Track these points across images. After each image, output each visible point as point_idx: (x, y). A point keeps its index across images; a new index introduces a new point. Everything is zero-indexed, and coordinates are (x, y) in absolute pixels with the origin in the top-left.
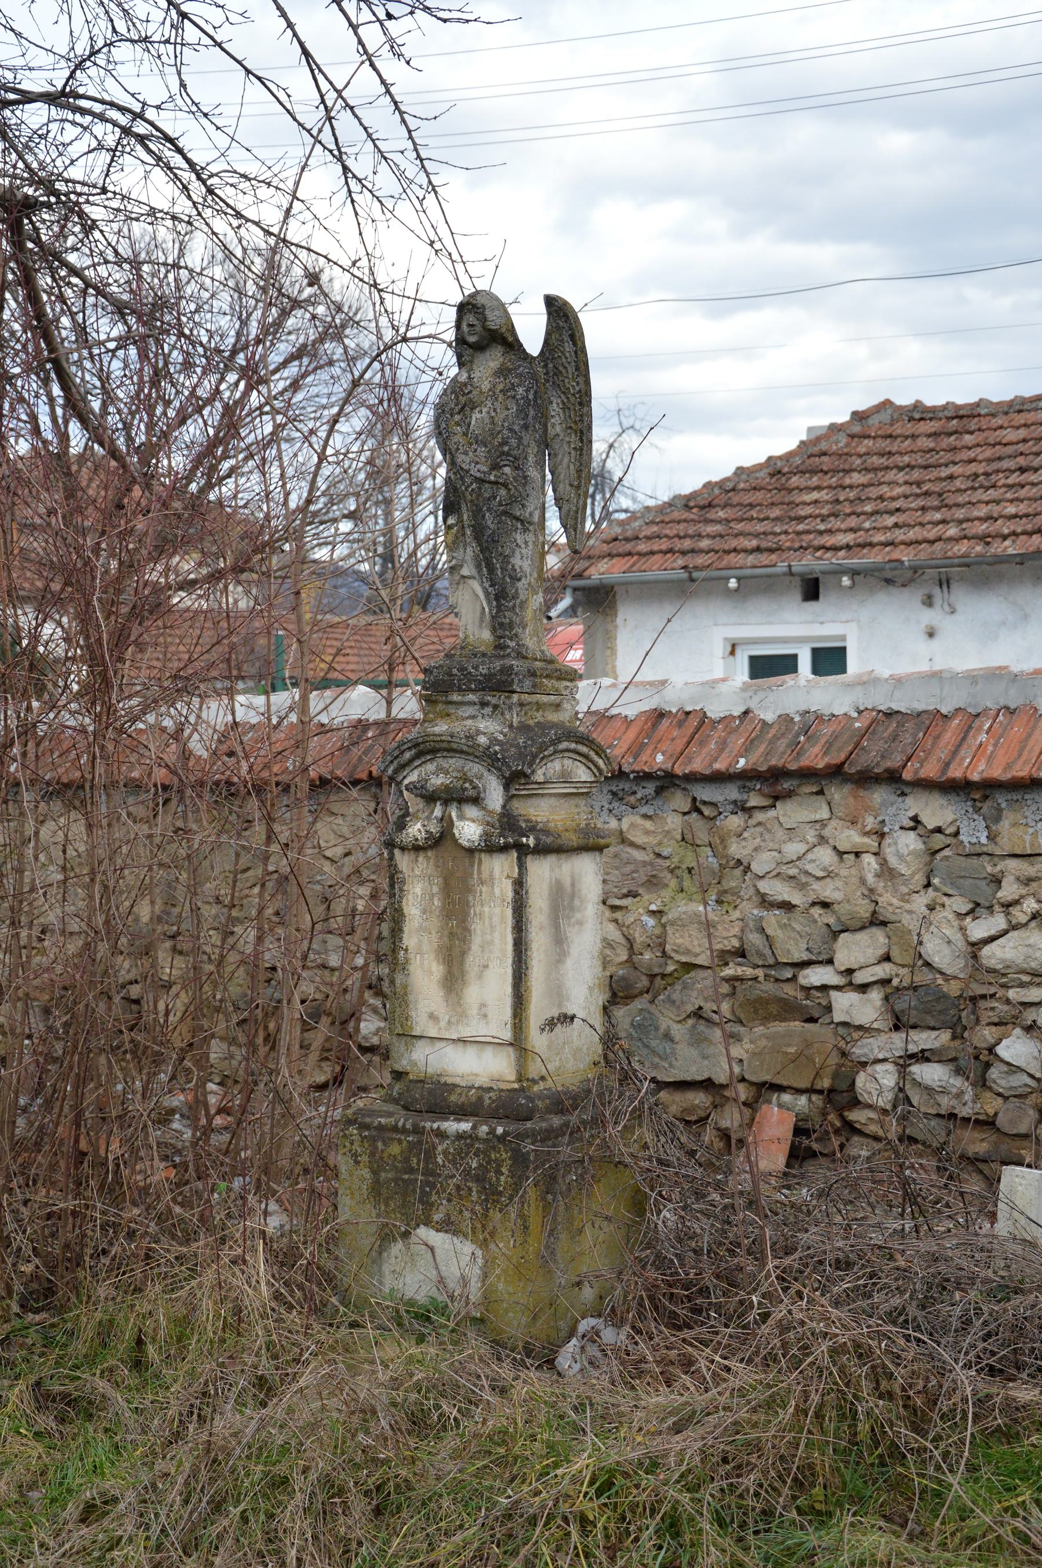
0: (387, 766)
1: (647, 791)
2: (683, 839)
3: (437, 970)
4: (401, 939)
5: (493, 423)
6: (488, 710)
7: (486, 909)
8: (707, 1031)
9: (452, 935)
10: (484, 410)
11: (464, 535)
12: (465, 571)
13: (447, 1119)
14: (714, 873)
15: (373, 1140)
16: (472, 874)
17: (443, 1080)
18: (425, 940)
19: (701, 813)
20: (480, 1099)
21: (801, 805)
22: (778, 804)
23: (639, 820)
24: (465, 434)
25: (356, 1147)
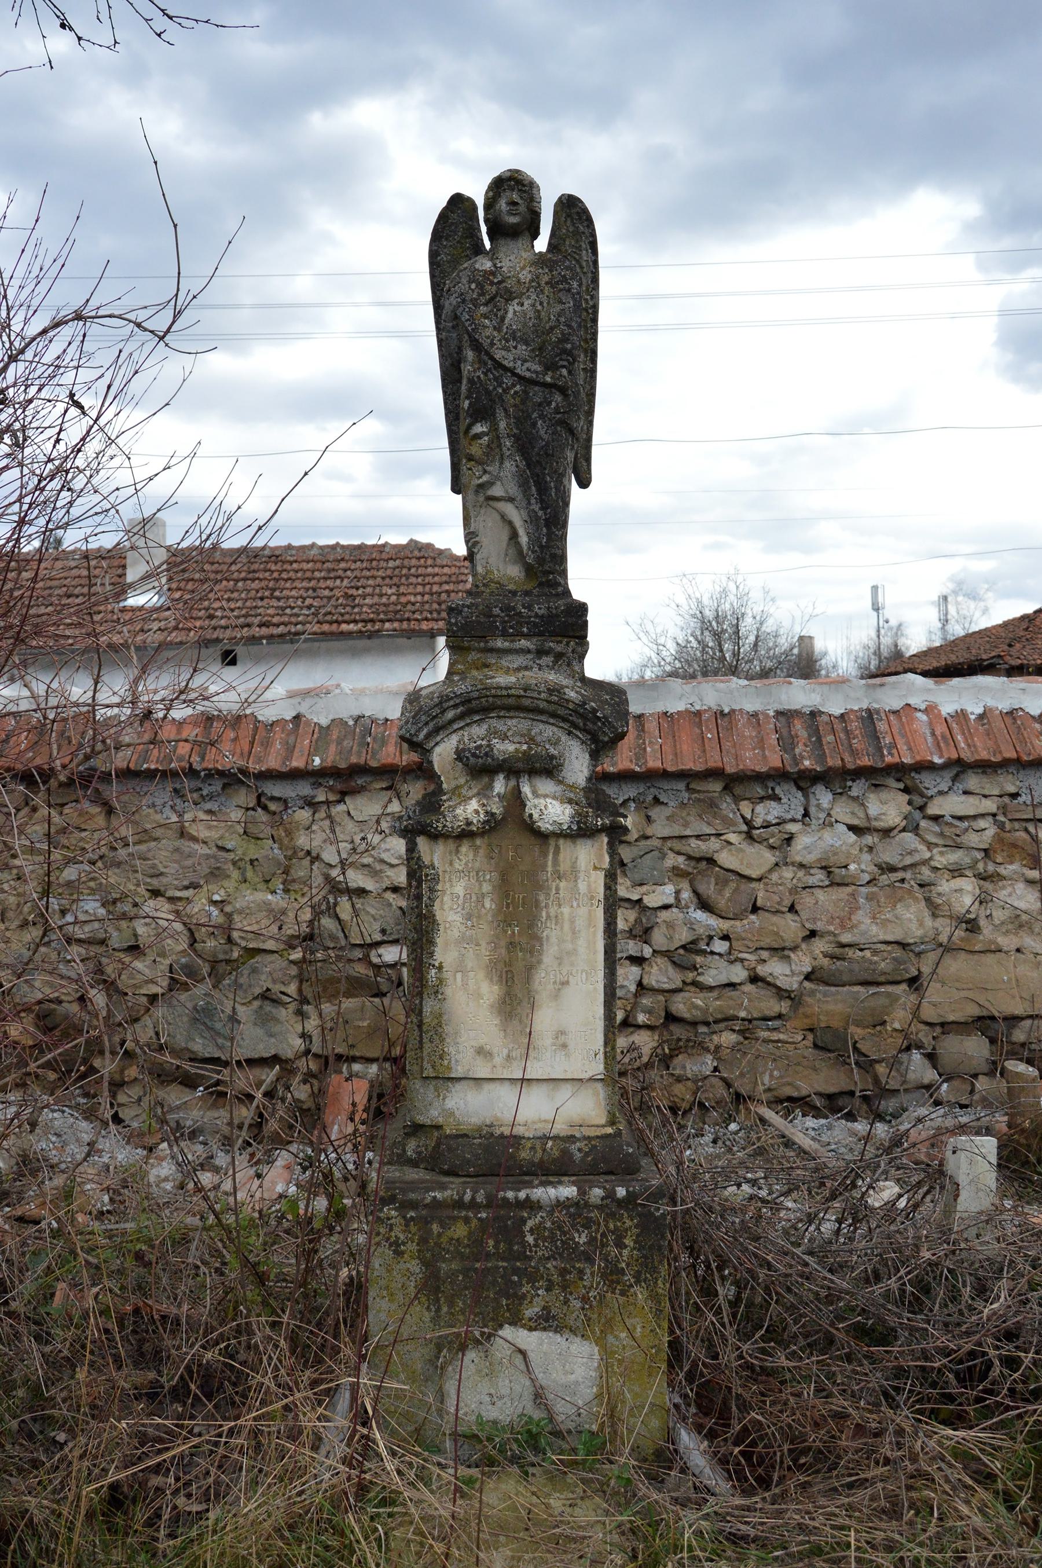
0: (420, 730)
1: (213, 788)
2: (245, 832)
3: (490, 991)
5: (538, 318)
6: (547, 660)
7: (566, 910)
8: (274, 1011)
9: (512, 945)
10: (527, 303)
11: (500, 446)
12: (497, 491)
13: (530, 1185)
14: (279, 864)
15: (426, 1222)
16: (545, 865)
17: (497, 1132)
18: (470, 954)
19: (265, 808)
21: (370, 799)
22: (347, 799)
23: (202, 816)
24: (498, 329)
25: (397, 1232)
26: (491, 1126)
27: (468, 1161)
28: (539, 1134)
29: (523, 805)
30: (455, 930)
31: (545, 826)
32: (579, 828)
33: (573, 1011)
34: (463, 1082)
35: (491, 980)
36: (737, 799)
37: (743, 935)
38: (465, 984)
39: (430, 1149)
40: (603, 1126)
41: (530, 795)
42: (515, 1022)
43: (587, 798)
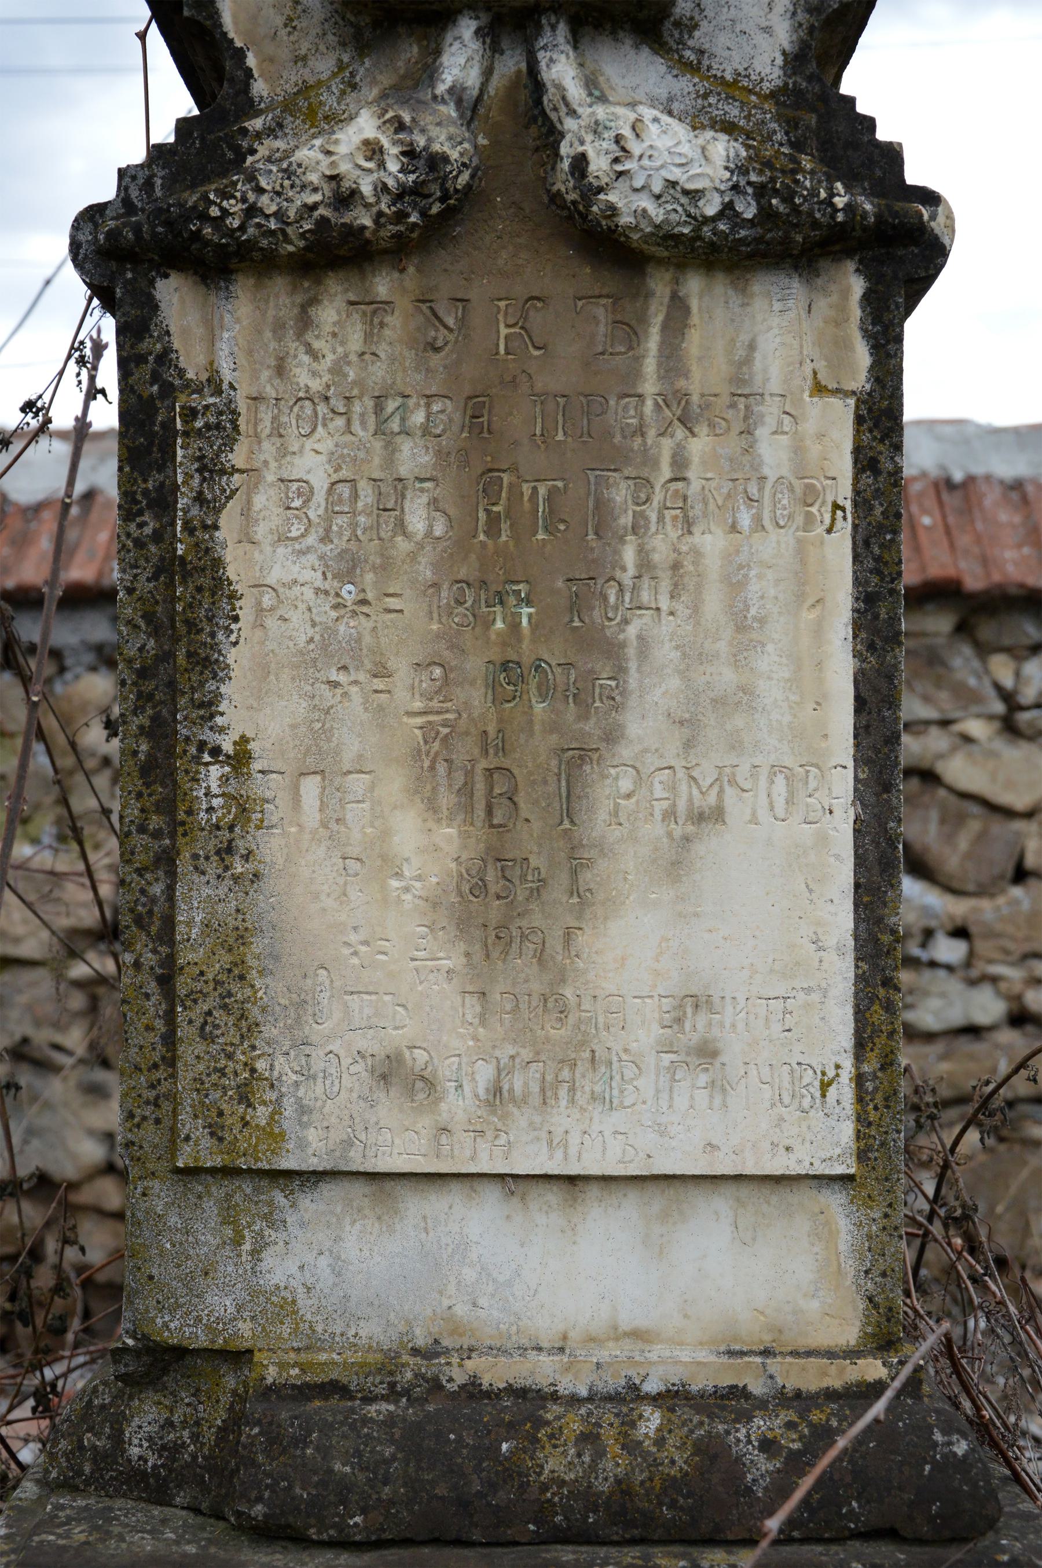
3: (426, 846)
4: (208, 708)
7: (711, 542)
9: (508, 675)
16: (634, 374)
20: (711, 1454)
26: (431, 1352)
27: (344, 1490)
28: (613, 1382)
29: (552, 135)
30: (296, 617)
31: (632, 205)
32: (766, 214)
33: (737, 923)
34: (328, 1190)
35: (432, 806)
36: (984, 650)
37: (999, 927)
38: (333, 821)
39: (209, 1436)
40: (852, 1354)
41: (575, 91)
42: (523, 964)
43: (791, 125)
